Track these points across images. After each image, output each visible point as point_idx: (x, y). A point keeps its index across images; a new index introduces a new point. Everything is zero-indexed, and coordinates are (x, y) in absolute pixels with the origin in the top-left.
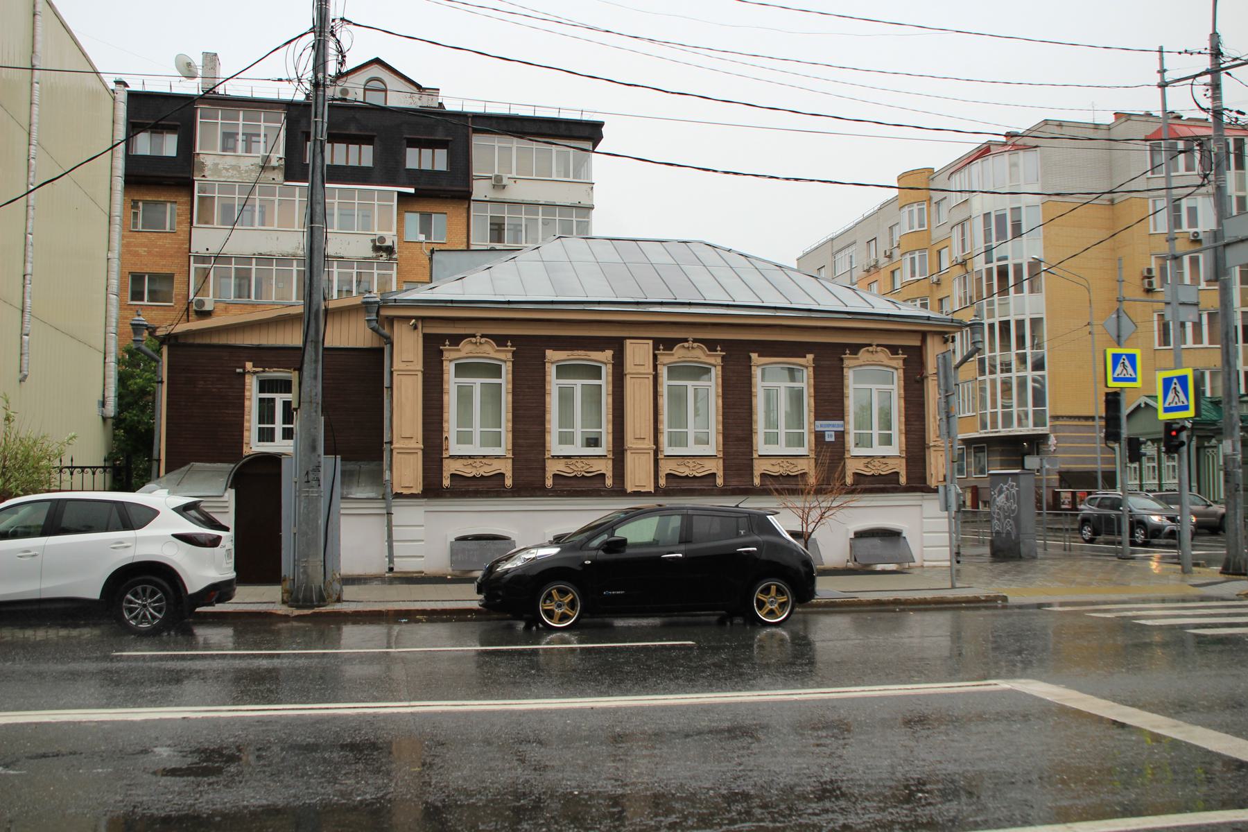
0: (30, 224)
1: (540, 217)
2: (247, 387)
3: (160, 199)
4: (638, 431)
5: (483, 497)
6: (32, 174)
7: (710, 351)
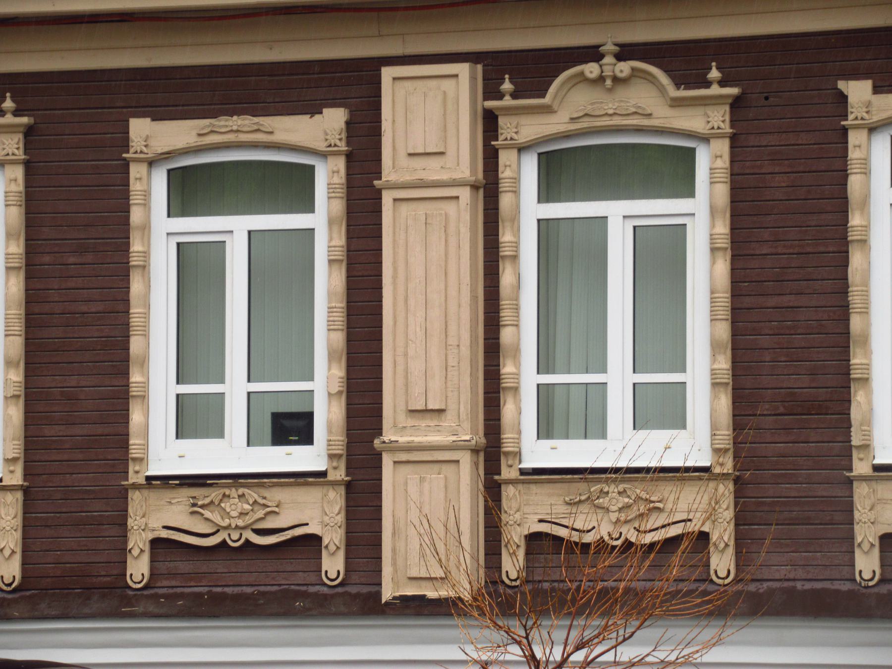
4: (417, 390)
7: (678, 86)
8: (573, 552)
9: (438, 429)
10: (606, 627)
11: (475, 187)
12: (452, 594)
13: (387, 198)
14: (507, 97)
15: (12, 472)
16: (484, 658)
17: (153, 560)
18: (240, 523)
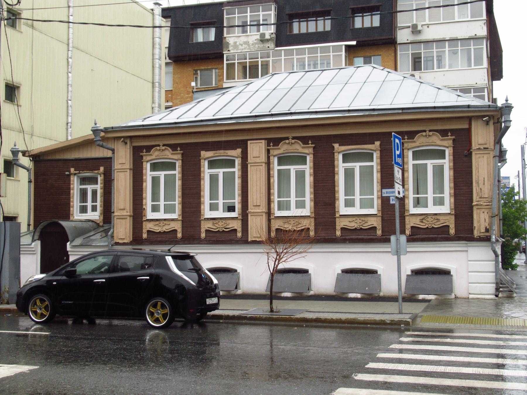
0: (69, 95)
1: (447, 49)
2: (71, 182)
3: (209, 68)
4: (255, 202)
5: (163, 245)
6: (70, 67)
7: (303, 144)
8: (284, 232)
9: (259, 209)
10: (290, 246)
11: (266, 163)
12: (261, 240)
13: (249, 165)
16: (268, 251)
17: (206, 233)
18: (222, 227)
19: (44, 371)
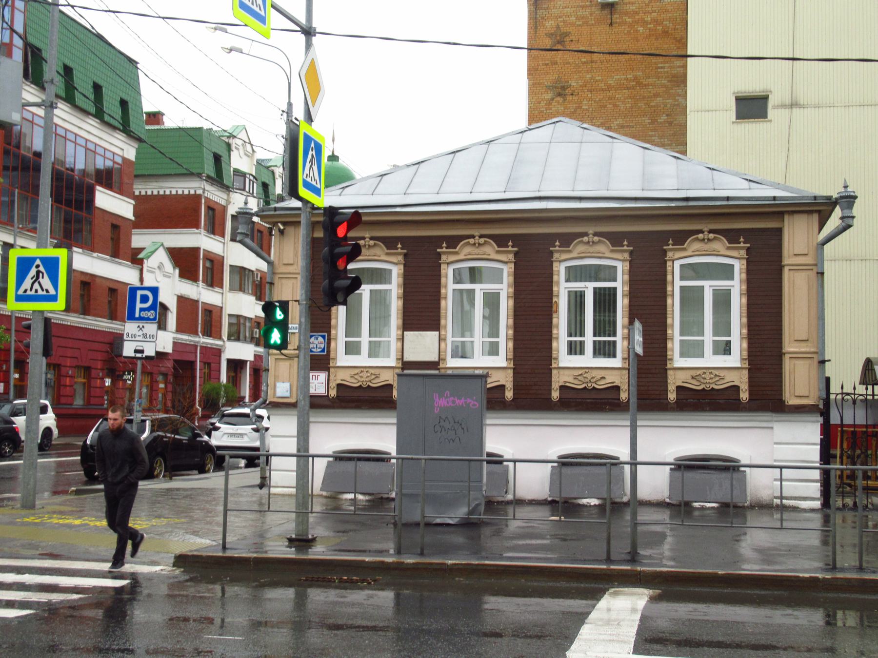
14: (399, 249)
15: (625, 363)
19: (141, 648)
